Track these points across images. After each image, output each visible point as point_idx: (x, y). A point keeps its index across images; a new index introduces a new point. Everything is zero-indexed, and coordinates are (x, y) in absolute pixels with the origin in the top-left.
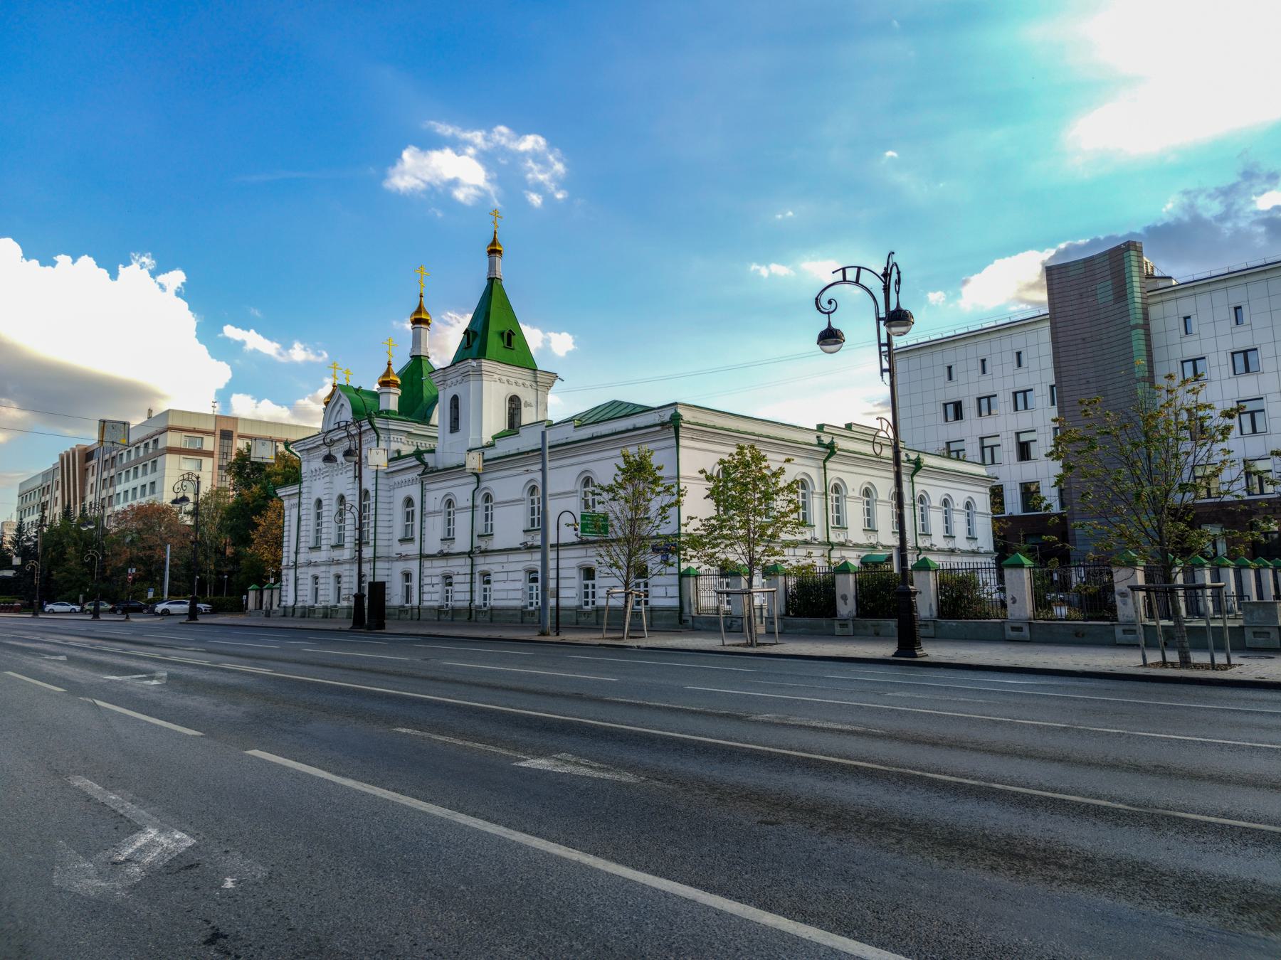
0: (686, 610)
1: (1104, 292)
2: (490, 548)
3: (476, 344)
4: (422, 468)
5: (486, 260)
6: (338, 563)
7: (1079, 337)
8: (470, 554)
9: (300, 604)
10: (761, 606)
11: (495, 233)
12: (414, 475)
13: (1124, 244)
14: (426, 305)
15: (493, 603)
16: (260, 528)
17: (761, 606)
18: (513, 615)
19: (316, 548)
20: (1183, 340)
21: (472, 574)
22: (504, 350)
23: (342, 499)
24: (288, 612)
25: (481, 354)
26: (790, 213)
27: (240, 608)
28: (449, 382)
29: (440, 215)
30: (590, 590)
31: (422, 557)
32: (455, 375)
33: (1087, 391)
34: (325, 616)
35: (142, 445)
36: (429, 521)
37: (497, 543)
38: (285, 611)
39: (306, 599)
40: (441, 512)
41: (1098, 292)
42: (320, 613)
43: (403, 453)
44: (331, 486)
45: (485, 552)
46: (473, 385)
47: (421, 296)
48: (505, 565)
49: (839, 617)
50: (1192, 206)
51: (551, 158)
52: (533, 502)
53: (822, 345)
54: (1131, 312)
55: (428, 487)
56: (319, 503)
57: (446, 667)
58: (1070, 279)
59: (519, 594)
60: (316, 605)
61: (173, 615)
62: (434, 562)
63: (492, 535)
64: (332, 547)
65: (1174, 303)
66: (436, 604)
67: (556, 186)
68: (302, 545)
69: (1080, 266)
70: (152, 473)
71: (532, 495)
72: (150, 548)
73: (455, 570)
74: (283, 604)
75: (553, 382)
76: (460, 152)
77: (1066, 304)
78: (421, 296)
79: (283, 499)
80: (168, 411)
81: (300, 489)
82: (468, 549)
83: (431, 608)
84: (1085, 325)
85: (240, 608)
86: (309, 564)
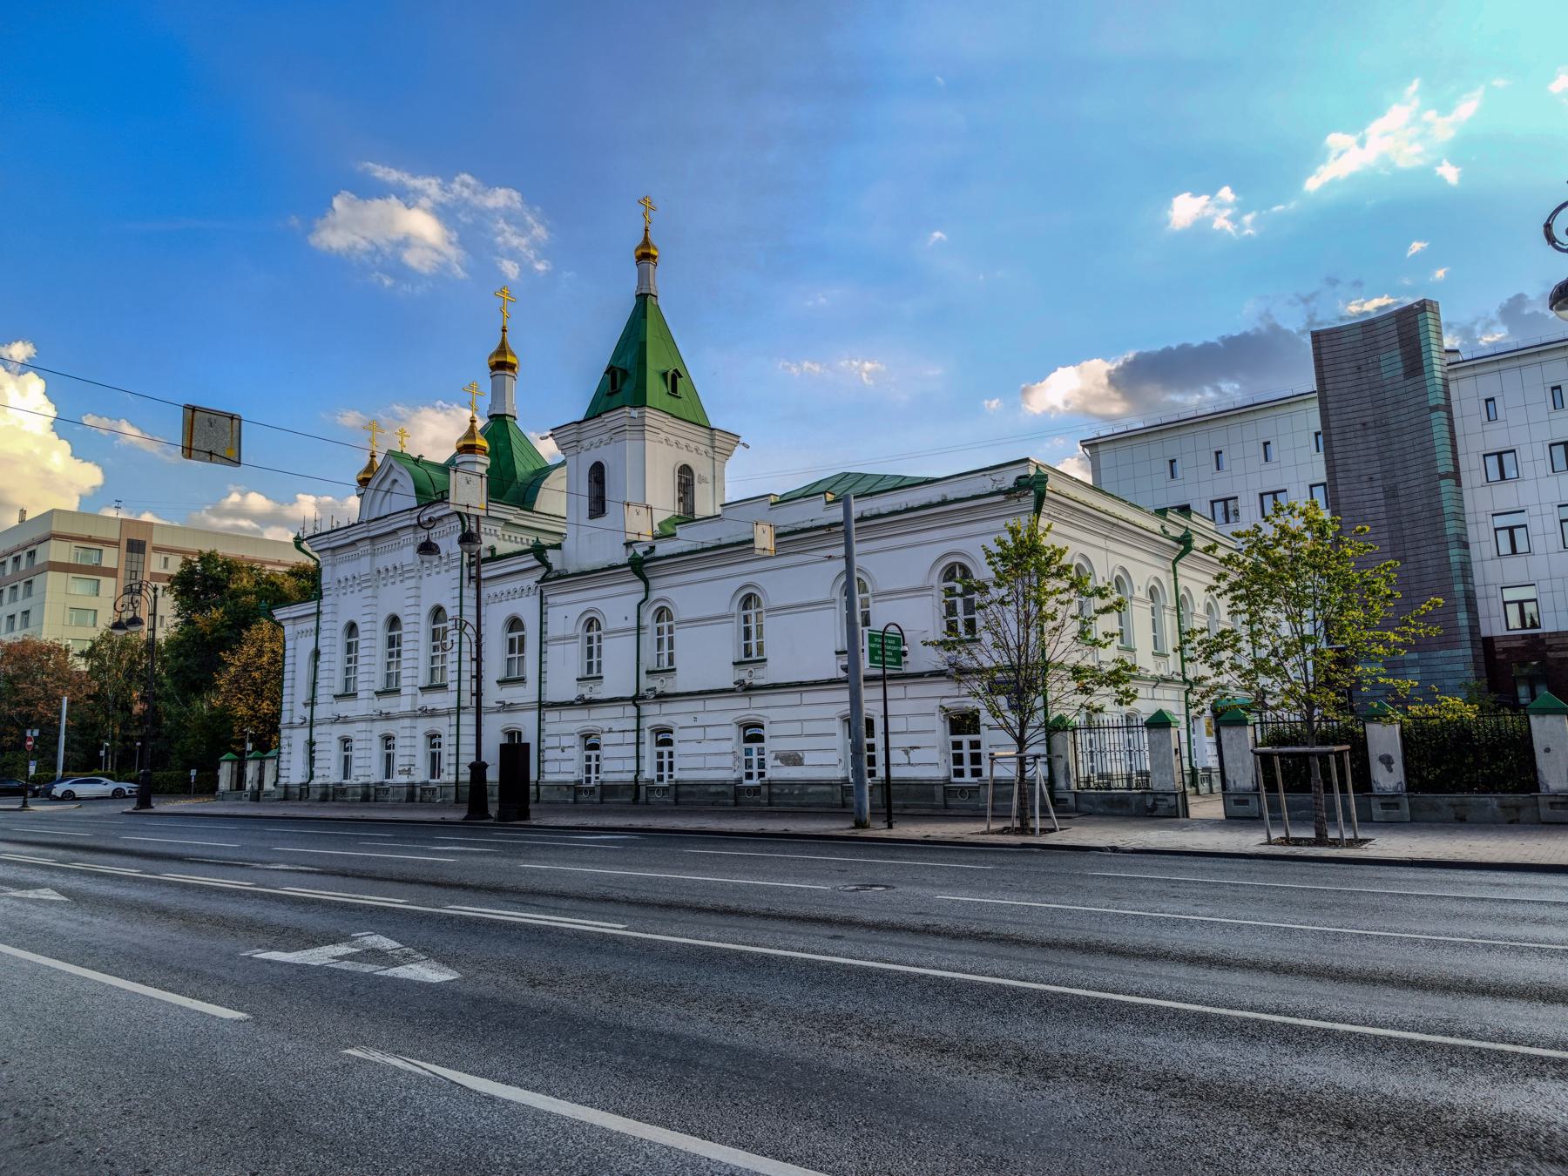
0: (1061, 783)
1: (1392, 364)
2: (668, 690)
3: (628, 387)
4: (543, 571)
5: (633, 271)
6: (432, 713)
7: (1358, 421)
8: (637, 700)
9: (317, 781)
10: (1089, 777)
11: (646, 230)
12: (530, 580)
13: (1418, 303)
14: (511, 343)
15: (677, 775)
16: (232, 669)
17: (1089, 777)
18: (717, 793)
19: (348, 694)
20: (1485, 428)
21: (638, 730)
22: (668, 397)
23: (438, 613)
24: (288, 794)
25: (639, 401)
26: (822, 300)
27: (208, 787)
28: (586, 443)
29: (388, 282)
30: (666, 760)
31: (542, 706)
32: (597, 431)
33: (1370, 491)
34: (366, 798)
35: (24, 555)
36: (553, 651)
37: (680, 683)
38: (286, 792)
39: (329, 772)
40: (577, 637)
41: (1382, 364)
42: (355, 794)
43: (498, 553)
44: (374, 601)
45: (662, 697)
46: (630, 446)
47: (504, 331)
48: (699, 716)
49: (1376, 792)
50: (1268, 314)
51: (529, 219)
52: (746, 619)
53: (1559, 309)
54: (1430, 389)
55: (550, 600)
56: (352, 628)
57: (534, 873)
58: (1342, 347)
59: (728, 761)
60: (348, 781)
61: (79, 799)
62: (909, 688)
63: (601, 678)
64: (377, 693)
65: (1472, 380)
66: (570, 778)
67: (535, 255)
68: (320, 691)
69: (1357, 331)
70: (10, 602)
71: (745, 608)
72: (28, 703)
73: (605, 725)
74: (282, 781)
75: (731, 451)
76: (411, 204)
77: (1340, 379)
78: (504, 331)
79: (284, 623)
80: (53, 511)
81: (318, 607)
82: (631, 693)
83: (559, 786)
84: (1364, 406)
85: (208, 787)
86: (337, 720)
